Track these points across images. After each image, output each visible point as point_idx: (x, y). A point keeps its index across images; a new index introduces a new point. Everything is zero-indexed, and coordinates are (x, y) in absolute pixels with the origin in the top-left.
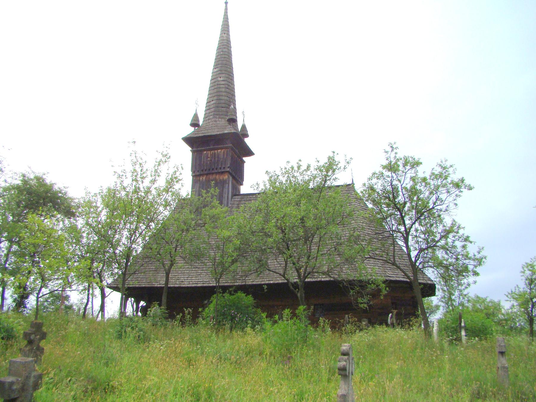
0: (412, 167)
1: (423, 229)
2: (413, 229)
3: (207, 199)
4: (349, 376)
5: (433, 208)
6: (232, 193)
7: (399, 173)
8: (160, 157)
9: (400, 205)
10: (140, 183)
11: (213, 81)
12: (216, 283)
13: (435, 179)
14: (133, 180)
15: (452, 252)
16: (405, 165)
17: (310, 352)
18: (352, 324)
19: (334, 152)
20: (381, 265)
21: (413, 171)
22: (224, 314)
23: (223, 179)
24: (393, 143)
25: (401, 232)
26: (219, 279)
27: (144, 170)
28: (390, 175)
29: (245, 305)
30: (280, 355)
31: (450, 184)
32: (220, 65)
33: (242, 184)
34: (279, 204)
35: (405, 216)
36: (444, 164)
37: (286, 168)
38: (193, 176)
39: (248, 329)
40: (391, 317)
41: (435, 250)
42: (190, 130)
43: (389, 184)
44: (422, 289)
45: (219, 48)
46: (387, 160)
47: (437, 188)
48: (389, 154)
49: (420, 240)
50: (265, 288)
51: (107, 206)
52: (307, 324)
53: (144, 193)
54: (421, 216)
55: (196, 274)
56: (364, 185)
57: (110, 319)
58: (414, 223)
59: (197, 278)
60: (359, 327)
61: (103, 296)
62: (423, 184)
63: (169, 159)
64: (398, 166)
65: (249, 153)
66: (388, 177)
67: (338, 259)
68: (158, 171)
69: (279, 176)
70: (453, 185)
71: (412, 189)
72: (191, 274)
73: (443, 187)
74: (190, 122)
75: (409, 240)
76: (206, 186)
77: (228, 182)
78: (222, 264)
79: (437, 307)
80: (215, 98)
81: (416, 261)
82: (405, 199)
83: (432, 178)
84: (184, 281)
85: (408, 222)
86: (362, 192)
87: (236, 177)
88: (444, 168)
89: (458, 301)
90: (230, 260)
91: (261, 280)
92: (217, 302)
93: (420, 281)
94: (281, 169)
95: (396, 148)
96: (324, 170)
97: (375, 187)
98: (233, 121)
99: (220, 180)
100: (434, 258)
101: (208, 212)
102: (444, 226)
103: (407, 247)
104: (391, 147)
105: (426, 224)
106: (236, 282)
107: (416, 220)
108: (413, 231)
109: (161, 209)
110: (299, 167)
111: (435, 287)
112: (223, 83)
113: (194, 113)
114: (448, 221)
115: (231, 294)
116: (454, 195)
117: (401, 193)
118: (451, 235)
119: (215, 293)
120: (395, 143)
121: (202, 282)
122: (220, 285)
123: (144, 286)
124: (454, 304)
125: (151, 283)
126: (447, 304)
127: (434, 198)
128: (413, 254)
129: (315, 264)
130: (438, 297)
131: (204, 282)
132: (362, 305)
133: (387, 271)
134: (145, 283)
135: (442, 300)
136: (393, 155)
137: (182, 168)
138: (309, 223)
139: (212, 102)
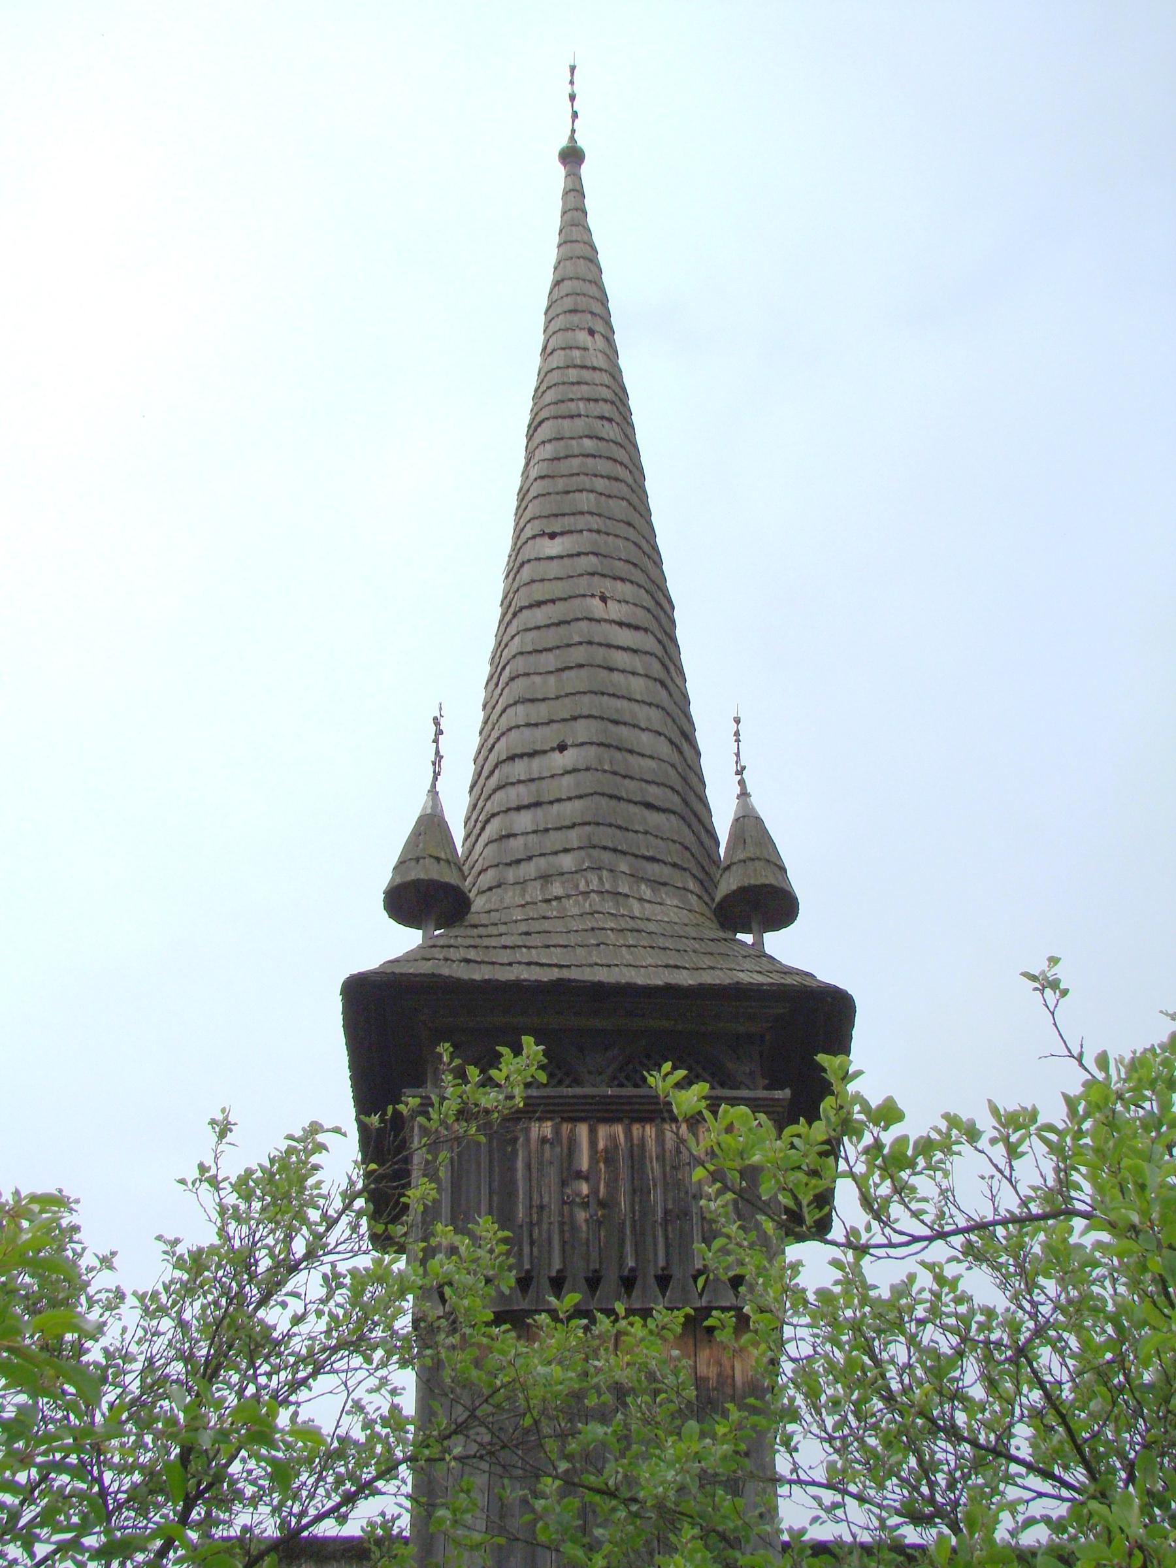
74: (383, 877)
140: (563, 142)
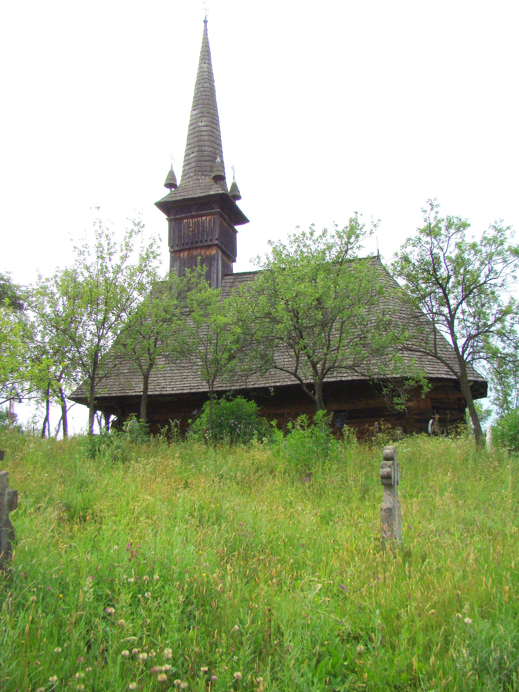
0: (458, 230)
1: (472, 310)
2: (459, 311)
3: (193, 280)
4: (394, 486)
5: (485, 282)
6: (223, 272)
7: (441, 238)
8: (131, 226)
9: (443, 279)
10: (107, 260)
11: (192, 127)
12: (209, 388)
13: (488, 245)
14: (98, 257)
15: (511, 338)
16: (448, 228)
17: (335, 467)
18: (384, 432)
19: (356, 213)
20: (417, 359)
21: (459, 235)
22: (220, 425)
23: (210, 255)
24: (433, 200)
25: (443, 315)
26: (213, 381)
27: (112, 244)
28: (430, 241)
29: (247, 414)
30: (297, 471)
31: (507, 251)
32: (201, 106)
33: (234, 261)
34: (290, 281)
35: (449, 293)
36: (499, 226)
37: (295, 235)
38: (171, 252)
39: (254, 441)
40: (432, 425)
41: (488, 336)
42: (164, 193)
43: (429, 253)
44: (472, 387)
45: (198, 83)
46: (425, 221)
47: (490, 257)
48: (428, 214)
49: (469, 324)
50: (272, 391)
51: (65, 293)
52: (327, 433)
53: (113, 273)
54: (470, 294)
55: (181, 377)
56: (396, 254)
57: (74, 438)
58: (461, 303)
59: (183, 383)
60: (392, 435)
61: (64, 410)
62: (472, 252)
63: (143, 229)
64: (440, 229)
65: (242, 219)
66: (427, 243)
67: (365, 352)
68: (130, 244)
69: (285, 246)
70: (511, 252)
71: (458, 259)
72: (175, 378)
73: (499, 254)
74: (164, 182)
75: (455, 325)
76: (191, 263)
77: (216, 258)
78: (217, 361)
79: (488, 413)
80: (196, 149)
81: (463, 352)
82: (449, 272)
83: (483, 244)
84: (165, 386)
85: (453, 302)
86: (393, 265)
87: (227, 251)
88: (499, 230)
89: (515, 403)
90: (226, 355)
91: (264, 382)
92: (211, 411)
93: (469, 378)
94: (289, 236)
95: (437, 206)
96: (344, 237)
97: (410, 257)
98: (220, 179)
99: (207, 256)
100: (487, 347)
101: (195, 296)
102: (499, 306)
103: (453, 334)
104: (431, 204)
105: (476, 304)
106: (233, 386)
107: (463, 299)
108: (459, 314)
109: (135, 294)
110: (312, 234)
111: (487, 386)
112: (205, 129)
113: (170, 169)
114: (504, 299)
115: (228, 400)
116: (512, 265)
117: (443, 264)
118: (508, 317)
119: (208, 399)
120: (435, 199)
121: (189, 388)
122: (214, 389)
123: (114, 395)
124: (511, 407)
125: (124, 391)
126: (501, 407)
127: (486, 270)
128: (461, 342)
129: (337, 357)
130: (490, 399)
131: (192, 387)
132: (399, 406)
133: (425, 366)
134: (116, 392)
135: (495, 402)
136: (432, 215)
137: (160, 239)
138: (329, 303)
139: (192, 155)
140: (204, 19)
